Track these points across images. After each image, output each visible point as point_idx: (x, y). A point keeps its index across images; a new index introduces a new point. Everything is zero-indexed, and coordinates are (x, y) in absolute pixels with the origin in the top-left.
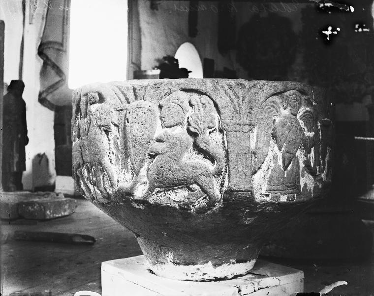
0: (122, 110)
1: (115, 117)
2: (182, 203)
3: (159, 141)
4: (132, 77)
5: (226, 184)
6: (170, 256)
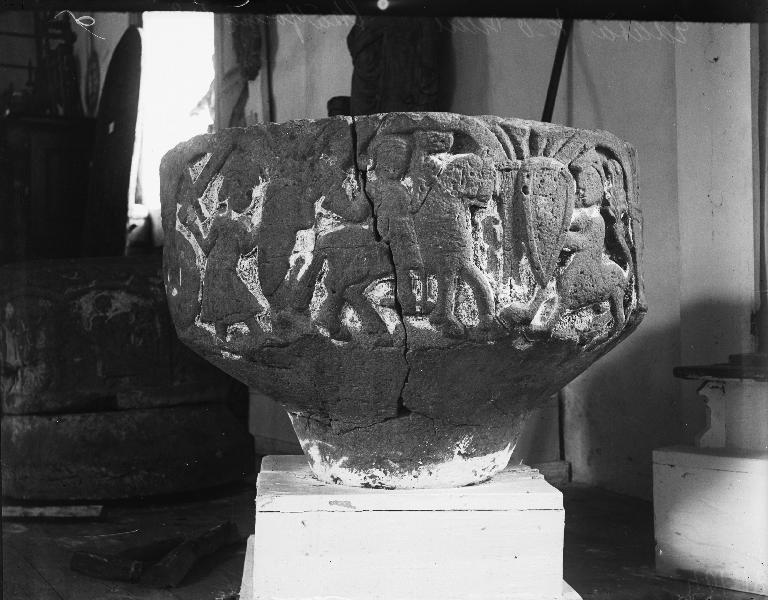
0: (508, 170)
1: (498, 184)
2: (586, 334)
3: (575, 229)
4: (541, 116)
5: (634, 300)
6: (462, 445)
